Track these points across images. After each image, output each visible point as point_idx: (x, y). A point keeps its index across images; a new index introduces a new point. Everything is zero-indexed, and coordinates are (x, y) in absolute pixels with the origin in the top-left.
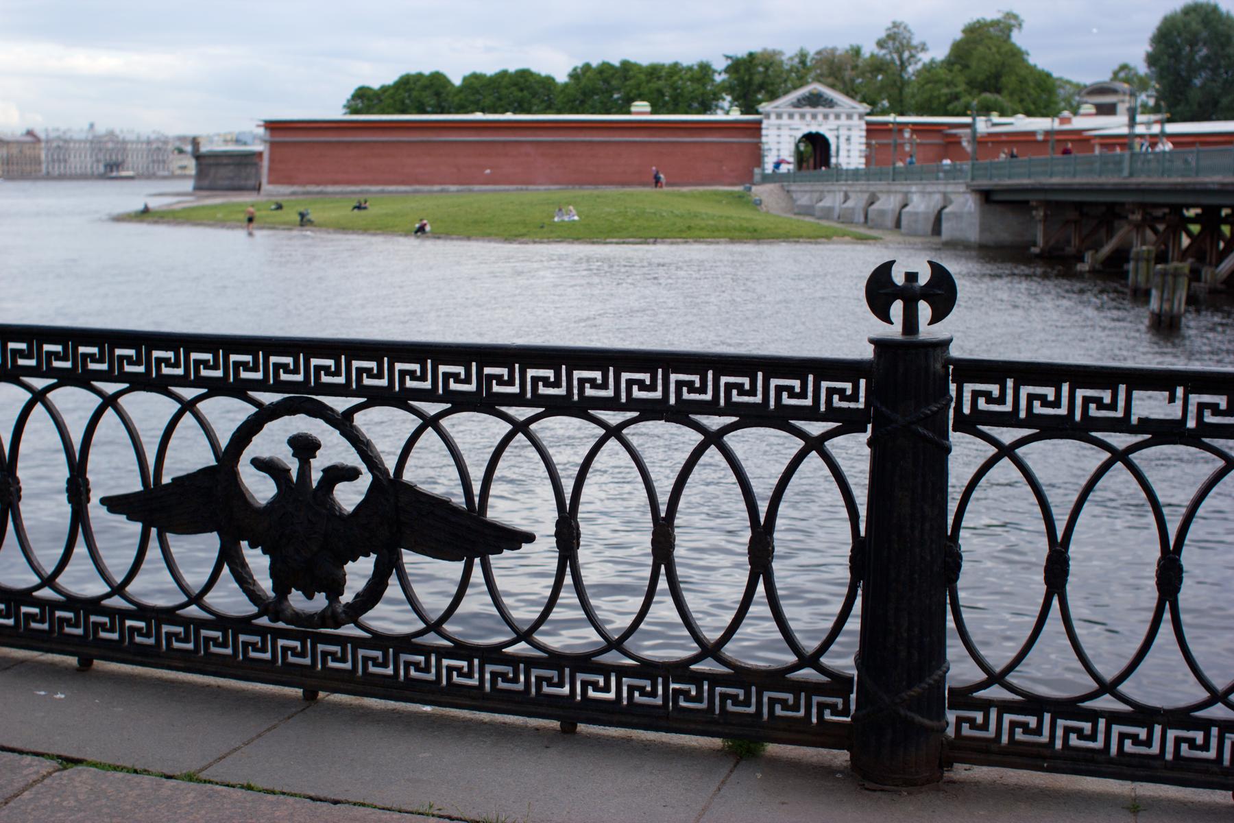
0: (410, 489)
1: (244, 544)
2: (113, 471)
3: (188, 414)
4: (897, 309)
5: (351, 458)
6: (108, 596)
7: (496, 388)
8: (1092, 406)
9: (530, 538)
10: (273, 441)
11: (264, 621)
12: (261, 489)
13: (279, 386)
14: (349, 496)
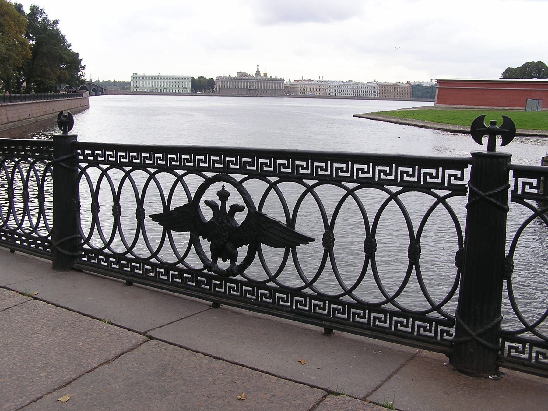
0: (264, 216)
1: (201, 238)
2: (154, 206)
3: (309, 194)
4: (485, 140)
5: (242, 203)
6: (304, 287)
7: (301, 171)
8: (459, 176)
9: (313, 240)
10: (211, 194)
11: (206, 271)
12: (208, 214)
13: (215, 170)
14: (240, 218)
